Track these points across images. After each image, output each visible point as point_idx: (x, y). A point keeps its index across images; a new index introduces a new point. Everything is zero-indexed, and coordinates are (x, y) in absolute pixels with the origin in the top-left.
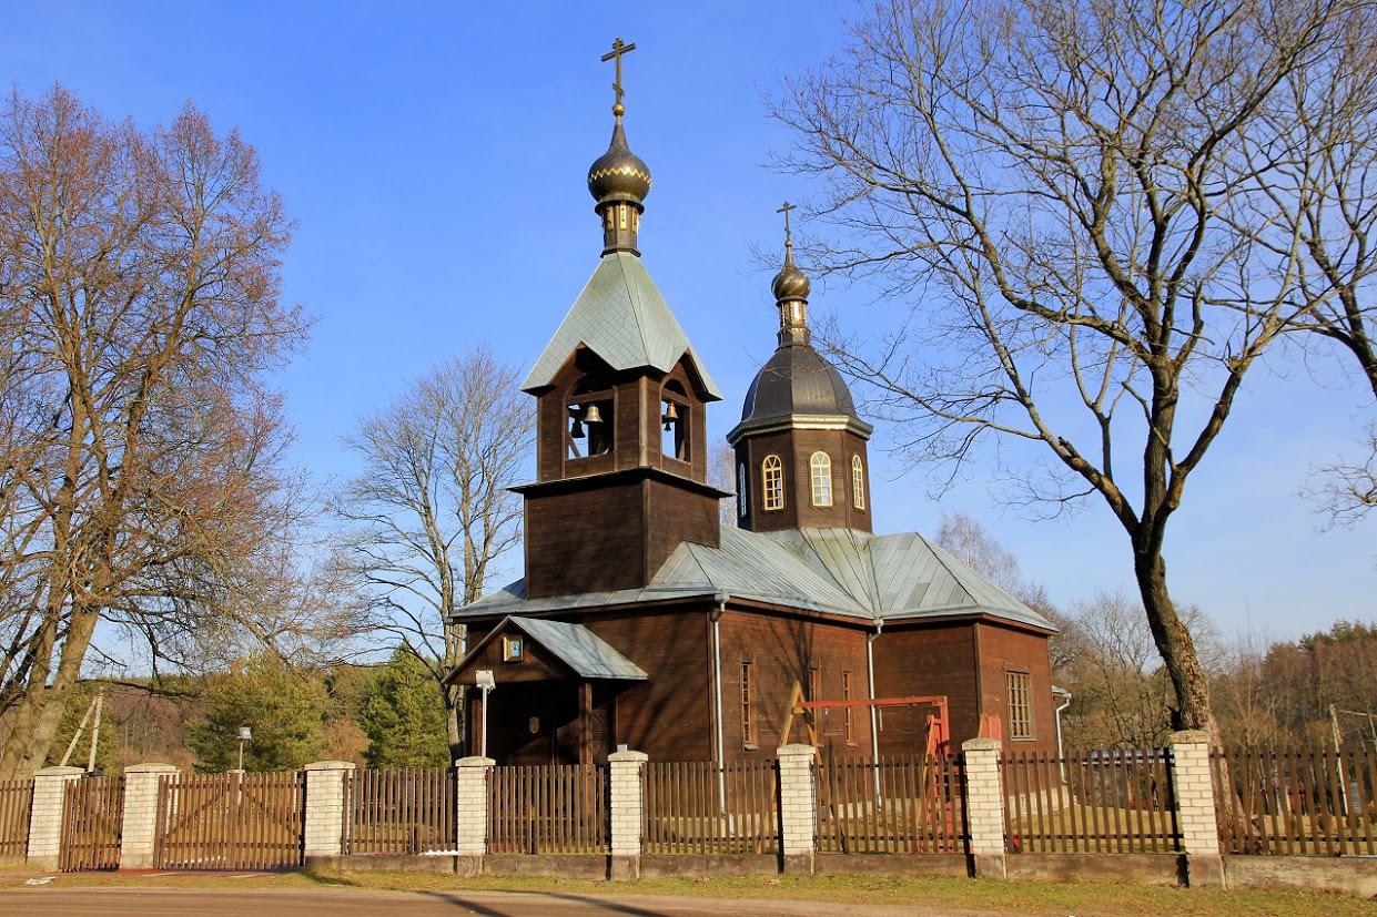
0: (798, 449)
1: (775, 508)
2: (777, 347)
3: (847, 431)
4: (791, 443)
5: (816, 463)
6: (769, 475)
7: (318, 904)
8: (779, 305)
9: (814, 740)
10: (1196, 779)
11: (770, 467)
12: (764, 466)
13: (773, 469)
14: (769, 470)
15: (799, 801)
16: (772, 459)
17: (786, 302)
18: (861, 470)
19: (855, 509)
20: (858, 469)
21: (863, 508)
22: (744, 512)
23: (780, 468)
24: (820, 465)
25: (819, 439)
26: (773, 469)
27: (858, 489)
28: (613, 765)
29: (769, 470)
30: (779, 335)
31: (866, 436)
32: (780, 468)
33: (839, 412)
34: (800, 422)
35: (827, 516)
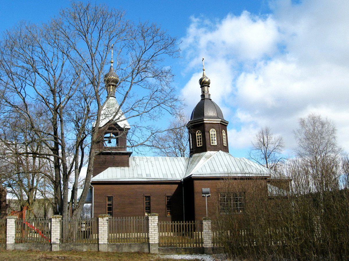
0: (206, 129)
1: (200, 146)
2: (201, 99)
3: (220, 123)
4: (204, 127)
5: (211, 132)
6: (198, 136)
7: (114, 229)
8: (201, 87)
9: (20, 247)
10: (154, 235)
11: (198, 134)
12: (196, 134)
13: (199, 135)
14: (198, 135)
15: (103, 237)
16: (199, 132)
17: (204, 86)
18: (225, 135)
19: (223, 146)
20: (224, 134)
21: (226, 146)
22: (191, 147)
23: (201, 134)
24: (213, 132)
25: (212, 125)
26: (199, 135)
27: (224, 140)
28: (8, 219)
29: (198, 135)
30: (201, 96)
31: (226, 125)
32: (201, 134)
33: (218, 118)
34: (206, 121)
35: (215, 148)
